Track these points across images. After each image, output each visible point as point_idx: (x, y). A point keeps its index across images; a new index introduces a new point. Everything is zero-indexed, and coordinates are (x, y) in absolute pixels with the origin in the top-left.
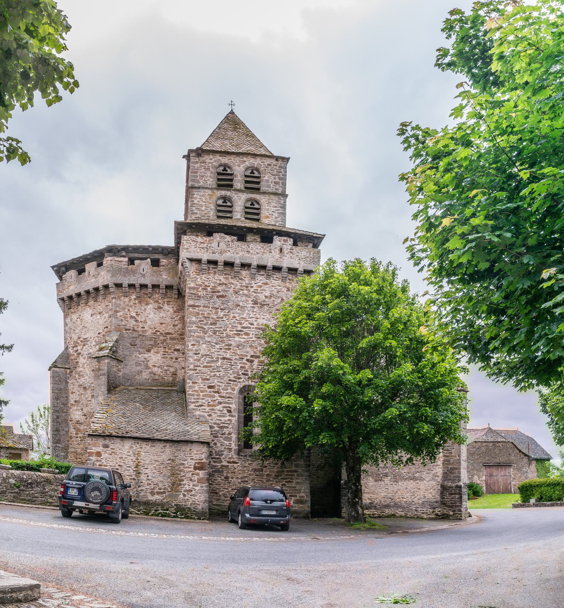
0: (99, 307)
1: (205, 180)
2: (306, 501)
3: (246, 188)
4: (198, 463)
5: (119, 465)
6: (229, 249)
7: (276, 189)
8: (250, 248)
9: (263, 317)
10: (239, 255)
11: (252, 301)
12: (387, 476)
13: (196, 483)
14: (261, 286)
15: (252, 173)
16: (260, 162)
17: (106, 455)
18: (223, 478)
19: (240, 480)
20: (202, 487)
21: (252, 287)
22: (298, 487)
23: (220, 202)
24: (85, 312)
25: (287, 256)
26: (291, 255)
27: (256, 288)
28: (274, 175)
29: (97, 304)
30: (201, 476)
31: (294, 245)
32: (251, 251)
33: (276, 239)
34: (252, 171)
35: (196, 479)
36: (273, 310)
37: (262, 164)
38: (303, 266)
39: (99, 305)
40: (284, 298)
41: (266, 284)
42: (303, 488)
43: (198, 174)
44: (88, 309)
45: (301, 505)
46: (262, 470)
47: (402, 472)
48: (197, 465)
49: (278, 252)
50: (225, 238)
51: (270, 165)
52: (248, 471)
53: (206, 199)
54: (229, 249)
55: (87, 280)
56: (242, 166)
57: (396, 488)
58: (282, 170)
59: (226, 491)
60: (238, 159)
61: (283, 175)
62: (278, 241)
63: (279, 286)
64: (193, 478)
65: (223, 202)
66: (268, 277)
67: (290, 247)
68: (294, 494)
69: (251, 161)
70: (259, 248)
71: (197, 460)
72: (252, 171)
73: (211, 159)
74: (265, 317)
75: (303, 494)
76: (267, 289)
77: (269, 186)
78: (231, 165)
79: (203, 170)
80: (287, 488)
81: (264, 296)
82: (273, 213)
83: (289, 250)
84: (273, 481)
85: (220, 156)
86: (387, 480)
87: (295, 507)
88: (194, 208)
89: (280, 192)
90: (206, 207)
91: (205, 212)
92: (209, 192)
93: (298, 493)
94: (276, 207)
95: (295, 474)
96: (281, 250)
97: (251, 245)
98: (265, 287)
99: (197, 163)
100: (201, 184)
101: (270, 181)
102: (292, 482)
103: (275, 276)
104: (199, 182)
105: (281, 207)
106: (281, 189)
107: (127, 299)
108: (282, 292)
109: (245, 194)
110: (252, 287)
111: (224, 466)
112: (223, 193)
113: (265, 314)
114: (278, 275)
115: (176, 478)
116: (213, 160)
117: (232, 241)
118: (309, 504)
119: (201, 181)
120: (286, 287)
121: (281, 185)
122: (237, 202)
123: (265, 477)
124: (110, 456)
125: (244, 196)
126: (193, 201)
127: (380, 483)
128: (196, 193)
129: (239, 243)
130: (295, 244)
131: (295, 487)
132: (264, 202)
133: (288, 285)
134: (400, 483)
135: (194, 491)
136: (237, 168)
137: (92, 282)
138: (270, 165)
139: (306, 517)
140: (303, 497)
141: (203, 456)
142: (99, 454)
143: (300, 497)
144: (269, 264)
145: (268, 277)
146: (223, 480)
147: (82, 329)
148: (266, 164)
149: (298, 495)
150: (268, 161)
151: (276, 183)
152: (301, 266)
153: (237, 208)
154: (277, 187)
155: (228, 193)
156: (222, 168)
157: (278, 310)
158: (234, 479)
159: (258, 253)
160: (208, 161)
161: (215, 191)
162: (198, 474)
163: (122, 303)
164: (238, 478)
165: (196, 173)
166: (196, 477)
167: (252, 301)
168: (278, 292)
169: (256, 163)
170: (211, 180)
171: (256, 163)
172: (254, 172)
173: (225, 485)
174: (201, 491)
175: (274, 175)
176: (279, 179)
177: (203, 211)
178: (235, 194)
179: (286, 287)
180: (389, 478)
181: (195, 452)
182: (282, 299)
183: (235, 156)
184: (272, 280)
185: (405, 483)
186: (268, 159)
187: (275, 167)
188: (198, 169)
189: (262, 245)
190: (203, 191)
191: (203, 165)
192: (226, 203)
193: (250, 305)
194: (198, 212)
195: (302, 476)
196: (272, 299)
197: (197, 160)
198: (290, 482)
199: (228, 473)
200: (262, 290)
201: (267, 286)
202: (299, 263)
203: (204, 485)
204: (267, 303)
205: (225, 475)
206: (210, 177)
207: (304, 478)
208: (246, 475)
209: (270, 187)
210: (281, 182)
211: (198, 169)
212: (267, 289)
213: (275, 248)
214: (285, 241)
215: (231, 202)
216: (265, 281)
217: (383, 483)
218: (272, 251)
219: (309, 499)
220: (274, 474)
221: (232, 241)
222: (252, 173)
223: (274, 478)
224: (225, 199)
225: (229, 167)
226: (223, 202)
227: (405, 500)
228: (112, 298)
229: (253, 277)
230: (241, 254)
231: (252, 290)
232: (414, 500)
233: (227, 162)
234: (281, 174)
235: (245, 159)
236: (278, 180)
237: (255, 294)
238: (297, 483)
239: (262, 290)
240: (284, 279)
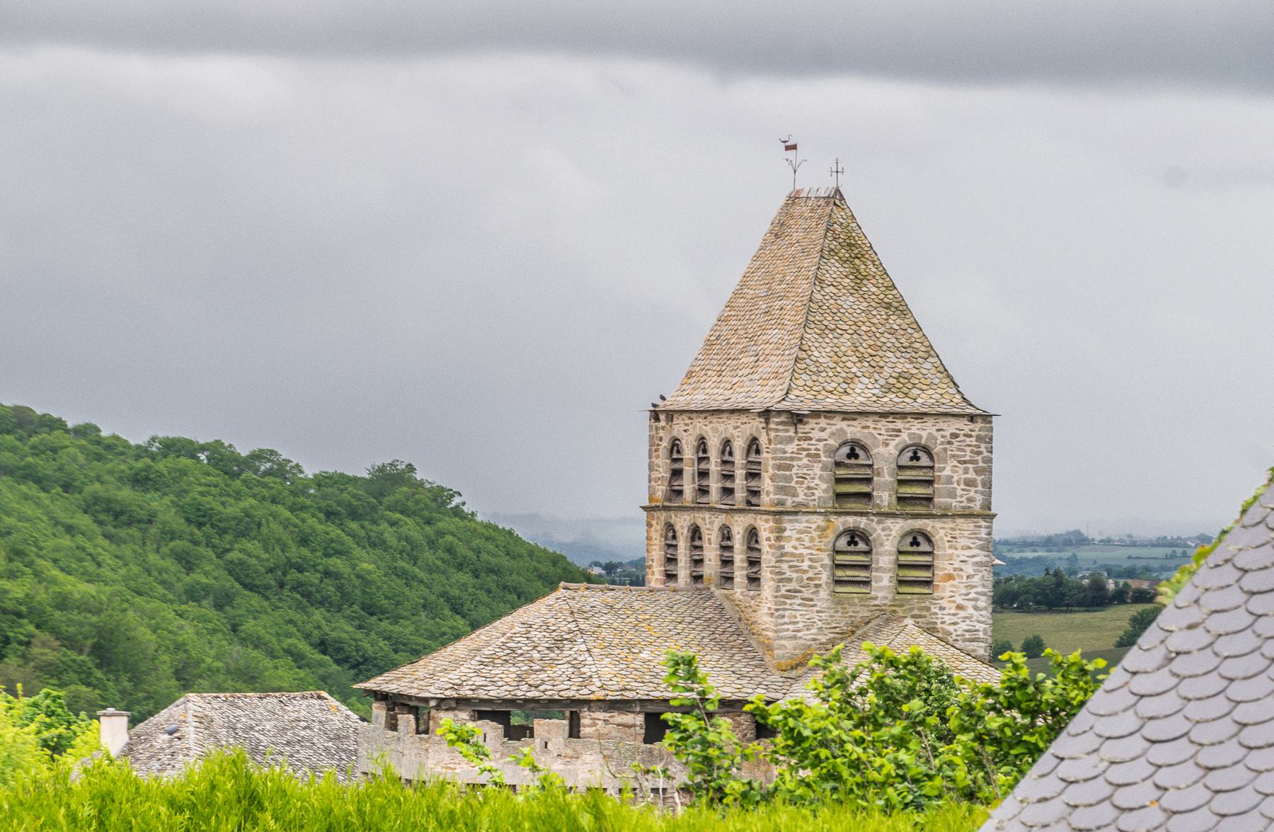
33: (540, 726)
225: (864, 448)
233: (858, 436)
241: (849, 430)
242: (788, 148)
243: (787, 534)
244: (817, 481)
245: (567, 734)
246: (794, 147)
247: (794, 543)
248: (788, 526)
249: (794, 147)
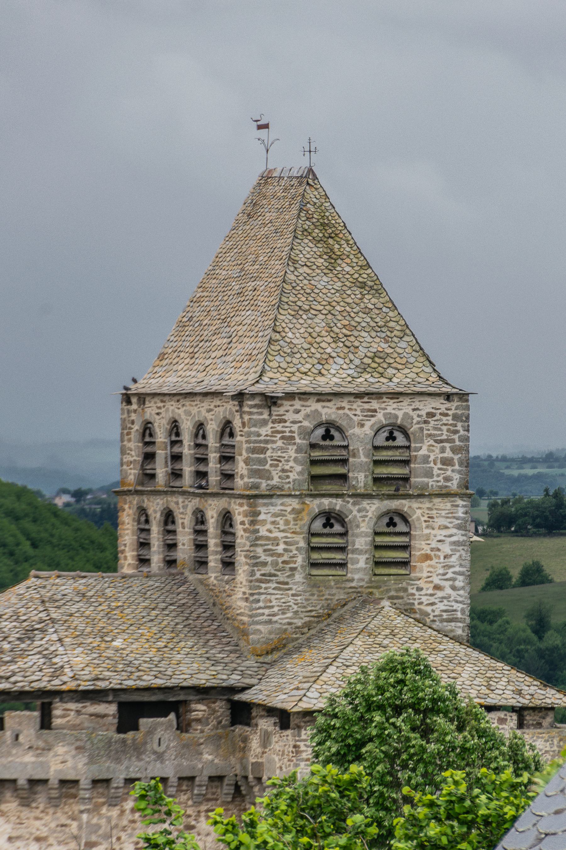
0: (38, 823)
29: (26, 813)
39: (37, 818)
107: (115, 812)
112: (326, 502)
137: (26, 764)
163: (103, 822)
225: (339, 429)
228: (82, 812)
241: (324, 411)
242: (260, 127)
244: (291, 464)
245: (38, 726)
246: (266, 126)
247: (269, 526)
249: (266, 126)
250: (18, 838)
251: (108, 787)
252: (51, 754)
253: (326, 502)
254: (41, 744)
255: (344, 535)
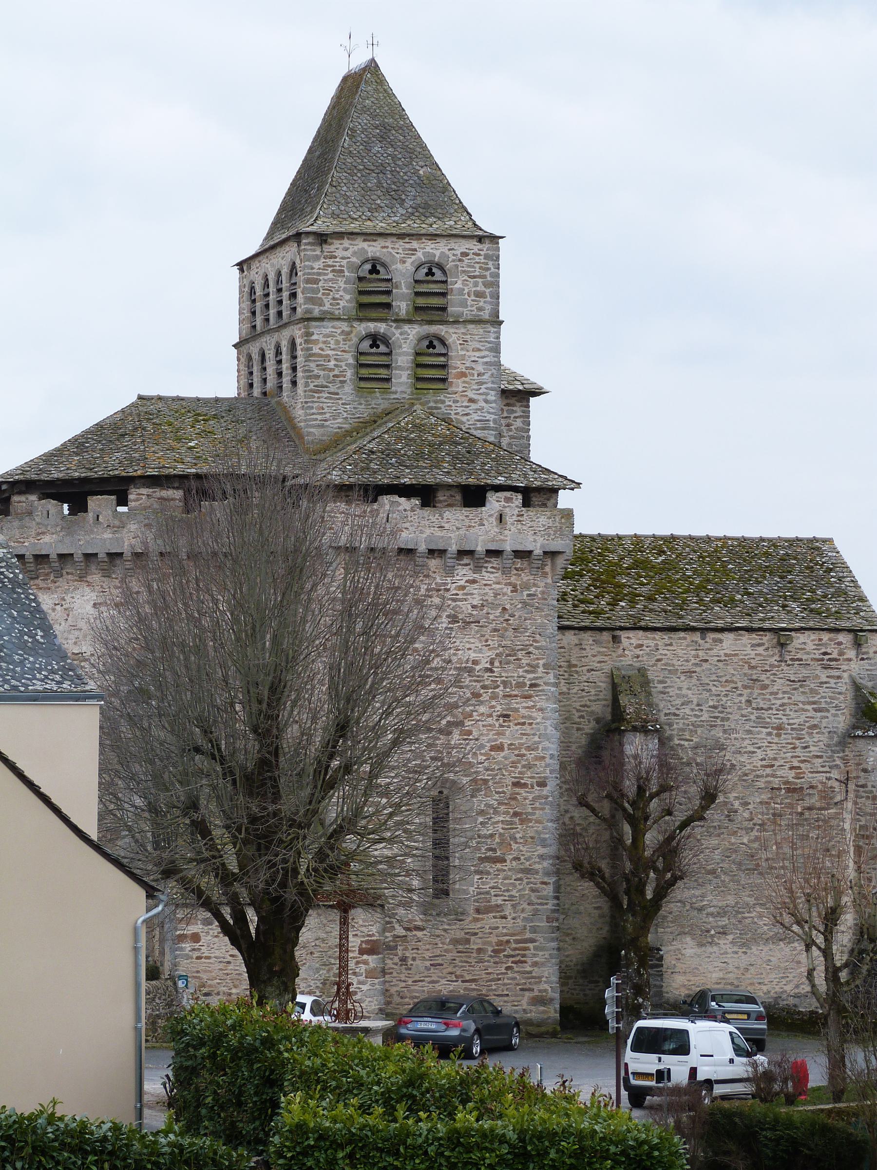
1: (334, 299)
2: (552, 1000)
3: (417, 309)
4: (367, 942)
5: (231, 956)
6: (406, 525)
7: (480, 309)
8: (445, 520)
9: (468, 646)
10: (425, 536)
11: (448, 616)
12: (725, 933)
13: (362, 978)
14: (463, 588)
15: (430, 273)
16: (445, 250)
17: (209, 938)
18: (396, 959)
19: (428, 963)
20: (373, 985)
21: (448, 590)
22: (536, 971)
23: (365, 345)
24: (77, 595)
25: (513, 529)
26: (519, 526)
27: (455, 592)
28: (474, 277)
30: (372, 965)
31: (524, 506)
32: (447, 526)
34: (430, 269)
35: (363, 971)
36: (487, 631)
37: (450, 254)
38: (542, 546)
40: (508, 607)
41: (474, 582)
42: (546, 974)
43: (321, 284)
44: (87, 589)
45: (542, 1008)
46: (468, 941)
47: (761, 923)
48: (364, 946)
49: (495, 523)
50: (400, 504)
51: (467, 255)
52: (443, 943)
53: (337, 342)
54: (406, 525)
55: (92, 532)
56: (409, 261)
57: (744, 960)
58: (490, 264)
59: (403, 984)
60: (400, 244)
61: (492, 275)
62: (494, 502)
63: (498, 583)
64: (357, 970)
65: (371, 346)
66: (478, 569)
67: (516, 512)
68: (528, 986)
69: (428, 249)
70: (461, 518)
71: (363, 936)
72: (430, 269)
73: (346, 249)
74: (472, 646)
75: (546, 986)
76: (475, 592)
77: (464, 304)
78: (385, 259)
79: (331, 276)
80: (516, 975)
81: (469, 607)
82: (473, 365)
83: (515, 518)
84: (488, 961)
85: (365, 240)
86: (725, 943)
87: (531, 1011)
88: (313, 365)
89: (485, 315)
90: (336, 359)
91: (336, 372)
92: (344, 326)
93: (536, 983)
94: (479, 350)
95: (531, 945)
96: (501, 518)
97: (447, 514)
98: (470, 588)
99: (317, 258)
100: (327, 307)
101: (466, 291)
102: (525, 962)
103: (491, 565)
104: (322, 304)
105: (490, 350)
106: (488, 307)
108: (504, 594)
109: (416, 326)
110: (448, 590)
111: (399, 937)
112: (372, 326)
113: (472, 640)
114: (495, 562)
115: (329, 971)
116: (351, 250)
117: (412, 510)
118: (558, 1006)
119: (325, 301)
120: (510, 584)
121: (488, 299)
122: (400, 347)
123: (475, 955)
124: (216, 939)
125: (413, 332)
126: (311, 349)
127: (709, 949)
128: (316, 331)
129: (427, 512)
130: (526, 503)
131: (531, 972)
132: (454, 342)
133: (513, 579)
134: (754, 948)
135: (359, 994)
136: (399, 266)
137: (105, 540)
138: (467, 255)
139: (554, 1035)
140: (546, 991)
141: (374, 930)
142: (196, 938)
143: (540, 991)
144: (479, 549)
145: (478, 569)
146: (396, 964)
147: (69, 632)
148: (458, 253)
149: (535, 987)
150: (463, 246)
151: (479, 295)
152: (539, 545)
153: (400, 359)
154: (481, 304)
155: (382, 327)
156: (368, 266)
157: (495, 630)
158: (418, 962)
159: (458, 528)
160: (340, 253)
161: (355, 324)
162: (366, 963)
164: (424, 959)
165: (316, 282)
166: (363, 968)
167: (448, 616)
168: (496, 595)
169: (438, 253)
170: (348, 297)
171: (438, 253)
172: (434, 270)
173: (401, 973)
174: (372, 992)
175: (474, 277)
176: (486, 285)
177: (331, 370)
178: (396, 328)
179: (510, 584)
180: (730, 937)
181: (361, 922)
182: (504, 609)
183: (394, 239)
184: (484, 574)
185: (766, 949)
186: (463, 241)
187: (477, 258)
188: (319, 274)
189: (466, 511)
190: (330, 324)
191: (330, 262)
192: (378, 347)
193: (444, 625)
194: (322, 373)
195: (542, 949)
196: (485, 610)
197: (318, 253)
198: (522, 962)
199: (406, 949)
200: (466, 594)
201: (475, 586)
202: (535, 541)
203: (376, 981)
204: (476, 619)
205: (400, 953)
206: (345, 290)
207: (547, 954)
208: (439, 953)
209: (467, 306)
210: (488, 291)
211: (319, 274)
212: (475, 592)
213: (491, 516)
214: (508, 500)
215: (387, 344)
216: (472, 576)
217: (715, 949)
218: (485, 522)
219: (557, 996)
220: (490, 949)
221: (412, 510)
222: (430, 273)
223: (491, 956)
224: (375, 339)
225: (384, 265)
226: (371, 346)
227: (765, 988)
229: (449, 571)
230: (428, 532)
231: (448, 595)
232: (786, 988)
234: (488, 273)
235: (415, 244)
236: (483, 289)
237: (454, 604)
238: (535, 964)
239: (466, 594)
240: (506, 571)
243: (314, 337)
248: (316, 331)
250: (100, 604)
251: (49, 562)
252: (125, 530)
253: (372, 326)
254: (117, 523)
255: (389, 354)
